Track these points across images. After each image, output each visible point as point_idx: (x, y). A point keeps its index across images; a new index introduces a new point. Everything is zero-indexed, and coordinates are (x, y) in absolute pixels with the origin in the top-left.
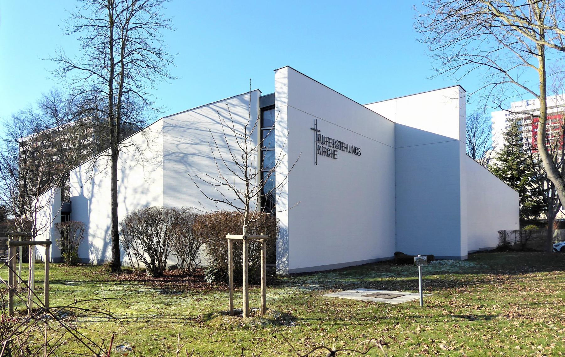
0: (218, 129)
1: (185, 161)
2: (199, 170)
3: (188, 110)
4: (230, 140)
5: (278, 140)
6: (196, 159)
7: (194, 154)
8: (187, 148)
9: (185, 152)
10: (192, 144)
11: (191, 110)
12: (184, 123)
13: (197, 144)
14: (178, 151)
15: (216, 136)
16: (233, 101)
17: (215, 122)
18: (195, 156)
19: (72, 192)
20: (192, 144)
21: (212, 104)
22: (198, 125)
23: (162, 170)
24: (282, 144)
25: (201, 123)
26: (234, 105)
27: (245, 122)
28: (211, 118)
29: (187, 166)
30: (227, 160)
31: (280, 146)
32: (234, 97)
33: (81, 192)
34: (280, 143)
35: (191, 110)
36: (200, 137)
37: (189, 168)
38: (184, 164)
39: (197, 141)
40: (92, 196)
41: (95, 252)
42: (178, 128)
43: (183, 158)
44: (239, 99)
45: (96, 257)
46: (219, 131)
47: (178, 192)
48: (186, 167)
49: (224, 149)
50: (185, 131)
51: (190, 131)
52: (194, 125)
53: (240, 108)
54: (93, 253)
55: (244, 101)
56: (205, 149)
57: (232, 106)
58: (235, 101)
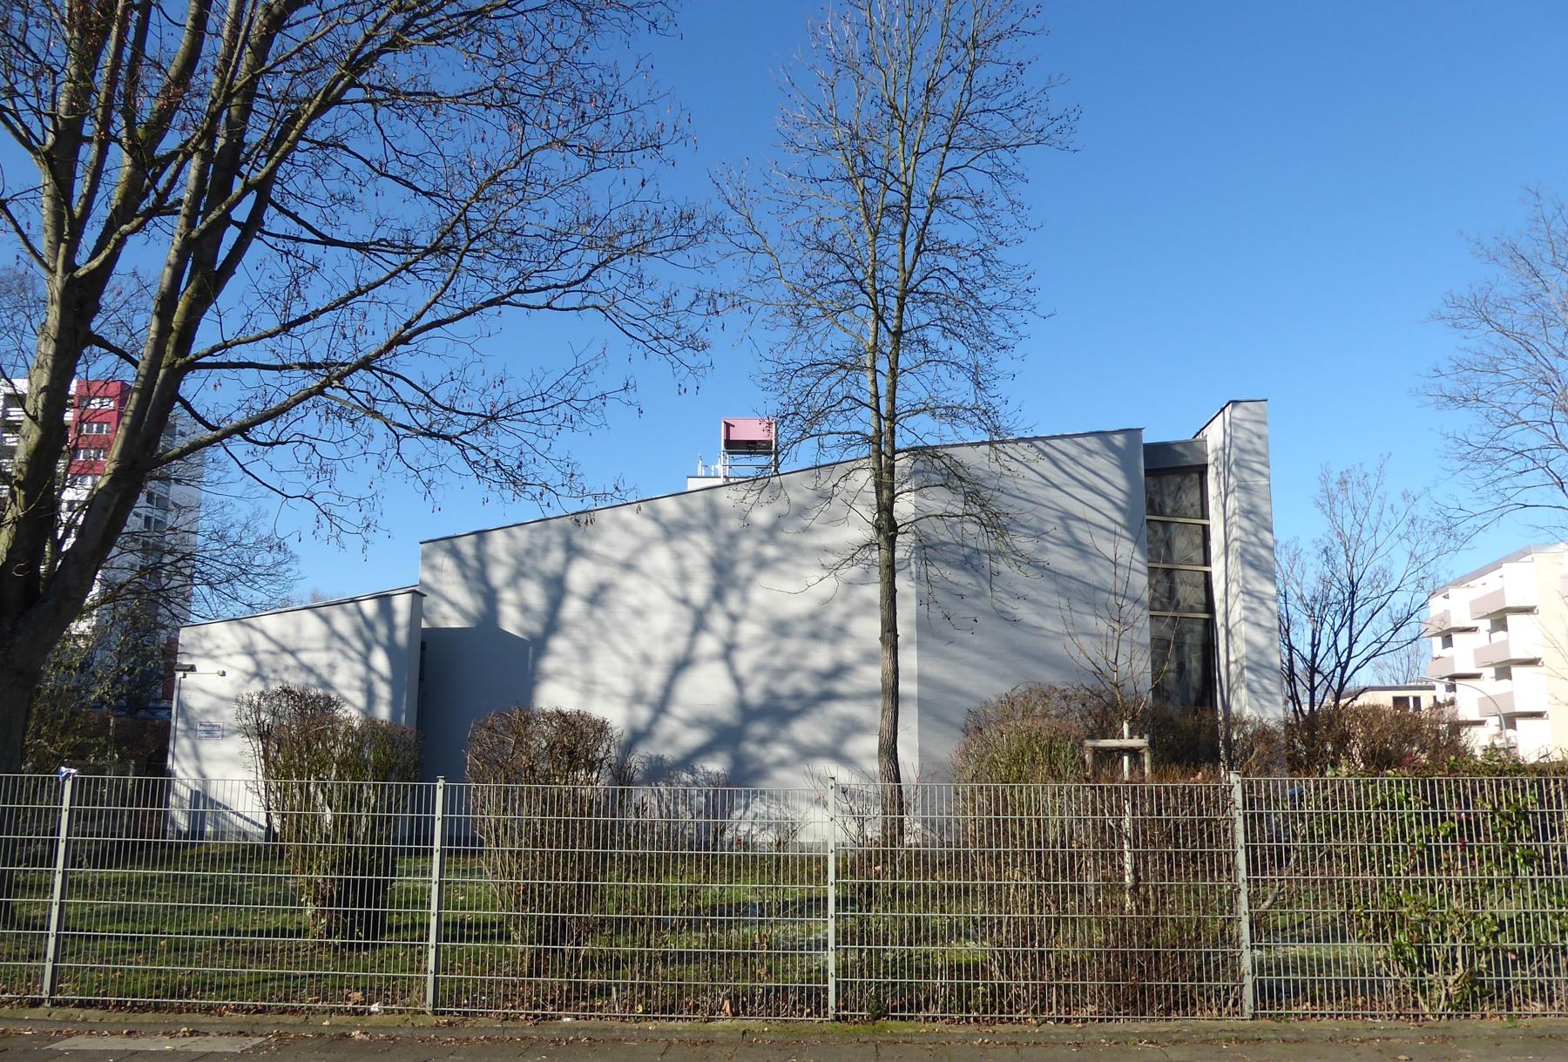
26: (1090, 452)
27: (1119, 497)
40: (553, 624)
58: (1092, 443)
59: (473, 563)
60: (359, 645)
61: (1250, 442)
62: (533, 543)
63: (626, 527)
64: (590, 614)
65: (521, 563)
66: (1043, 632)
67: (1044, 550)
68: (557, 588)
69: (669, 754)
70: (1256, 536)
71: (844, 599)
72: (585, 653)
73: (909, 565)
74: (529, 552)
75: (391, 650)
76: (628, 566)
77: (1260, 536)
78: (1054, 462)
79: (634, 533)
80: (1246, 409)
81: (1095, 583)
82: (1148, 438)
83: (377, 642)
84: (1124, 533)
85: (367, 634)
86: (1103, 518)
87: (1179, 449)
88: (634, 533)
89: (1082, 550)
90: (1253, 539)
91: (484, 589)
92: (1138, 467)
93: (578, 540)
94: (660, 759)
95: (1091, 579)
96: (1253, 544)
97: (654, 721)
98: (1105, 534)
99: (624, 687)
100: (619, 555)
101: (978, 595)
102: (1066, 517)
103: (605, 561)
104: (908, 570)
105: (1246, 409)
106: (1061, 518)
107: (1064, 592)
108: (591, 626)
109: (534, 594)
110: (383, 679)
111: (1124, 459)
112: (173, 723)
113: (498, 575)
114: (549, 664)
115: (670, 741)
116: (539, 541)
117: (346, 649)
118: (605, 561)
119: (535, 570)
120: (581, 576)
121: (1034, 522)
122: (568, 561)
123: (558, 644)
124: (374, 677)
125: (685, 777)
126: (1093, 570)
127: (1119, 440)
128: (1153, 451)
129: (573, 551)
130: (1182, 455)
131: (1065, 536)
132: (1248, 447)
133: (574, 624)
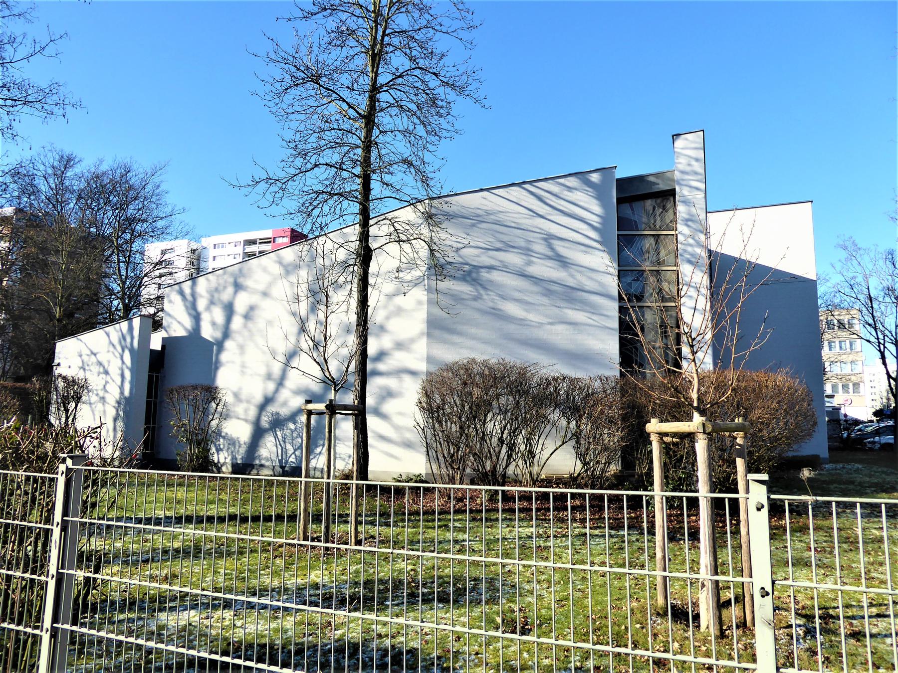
0: (541, 227)
1: (474, 280)
2: (503, 297)
3: (482, 190)
4: (564, 247)
5: (685, 251)
6: (495, 276)
7: (491, 268)
8: (478, 256)
9: (475, 264)
10: (489, 249)
11: (488, 190)
12: (472, 210)
13: (498, 250)
14: (461, 260)
15: (537, 238)
16: (568, 181)
17: (531, 213)
18: (495, 271)
19: (169, 326)
20: (489, 249)
21: (530, 183)
22: (501, 217)
23: (426, 293)
24: (696, 258)
25: (508, 214)
26: (569, 189)
27: (595, 220)
28: (526, 206)
29: (479, 288)
30: (558, 282)
31: (689, 262)
32: (570, 175)
33: (193, 329)
34: (688, 256)
35: (488, 190)
36: (506, 239)
37: (482, 292)
38: (472, 285)
39: (499, 245)
40: (226, 334)
41: (228, 448)
42: (460, 219)
43: (469, 273)
44: (579, 179)
45: (230, 458)
46: (542, 230)
47: (460, 334)
48: (477, 290)
49: (552, 261)
50: (473, 225)
51: (484, 225)
52: (492, 217)
53: (580, 193)
54: (222, 450)
55: (589, 184)
56: (514, 259)
57: (566, 188)
58: (572, 182)
59: (189, 298)
60: (119, 349)
61: (689, 165)
62: (219, 284)
63: (265, 270)
64: (245, 326)
65: (212, 296)
66: (528, 322)
67: (530, 263)
68: (229, 310)
69: (284, 412)
70: (693, 239)
71: (385, 307)
72: (242, 348)
73: (424, 280)
74: (217, 290)
75: (132, 350)
76: (265, 294)
77: (697, 238)
78: (540, 199)
79: (269, 273)
80: (686, 139)
81: (572, 285)
82: (620, 174)
83: (127, 347)
84: (598, 246)
85: (123, 342)
86: (580, 236)
87: (652, 179)
88: (269, 273)
89: (563, 262)
90: (691, 241)
91: (193, 313)
92: (611, 196)
93: (241, 280)
94: (278, 414)
95: (571, 282)
96: (691, 245)
97: (277, 391)
98: (582, 248)
99: (263, 371)
100: (261, 287)
101: (476, 299)
102: (549, 238)
103: (255, 292)
104: (423, 283)
105: (686, 139)
106: (545, 240)
107: (548, 293)
108: (246, 333)
109: (218, 315)
110: (127, 367)
111: (599, 192)
112: (612, 473)
113: (201, 305)
114: (224, 357)
115: (285, 404)
116: (221, 281)
117: (115, 351)
118: (255, 292)
119: (219, 300)
120: (242, 303)
121: (522, 244)
122: (236, 292)
123: (228, 344)
124: (124, 367)
125: (292, 426)
126: (572, 276)
127: (595, 177)
128: (622, 184)
129: (238, 287)
130: (655, 184)
131: (550, 253)
132: (688, 169)
133: (239, 332)
